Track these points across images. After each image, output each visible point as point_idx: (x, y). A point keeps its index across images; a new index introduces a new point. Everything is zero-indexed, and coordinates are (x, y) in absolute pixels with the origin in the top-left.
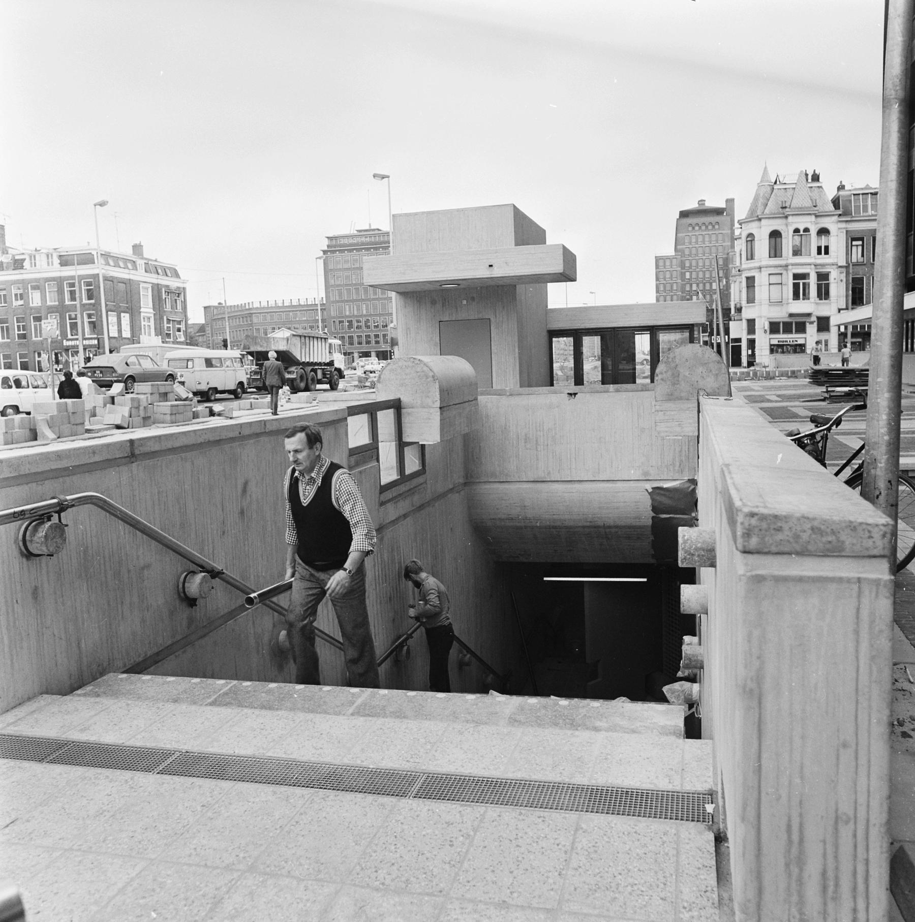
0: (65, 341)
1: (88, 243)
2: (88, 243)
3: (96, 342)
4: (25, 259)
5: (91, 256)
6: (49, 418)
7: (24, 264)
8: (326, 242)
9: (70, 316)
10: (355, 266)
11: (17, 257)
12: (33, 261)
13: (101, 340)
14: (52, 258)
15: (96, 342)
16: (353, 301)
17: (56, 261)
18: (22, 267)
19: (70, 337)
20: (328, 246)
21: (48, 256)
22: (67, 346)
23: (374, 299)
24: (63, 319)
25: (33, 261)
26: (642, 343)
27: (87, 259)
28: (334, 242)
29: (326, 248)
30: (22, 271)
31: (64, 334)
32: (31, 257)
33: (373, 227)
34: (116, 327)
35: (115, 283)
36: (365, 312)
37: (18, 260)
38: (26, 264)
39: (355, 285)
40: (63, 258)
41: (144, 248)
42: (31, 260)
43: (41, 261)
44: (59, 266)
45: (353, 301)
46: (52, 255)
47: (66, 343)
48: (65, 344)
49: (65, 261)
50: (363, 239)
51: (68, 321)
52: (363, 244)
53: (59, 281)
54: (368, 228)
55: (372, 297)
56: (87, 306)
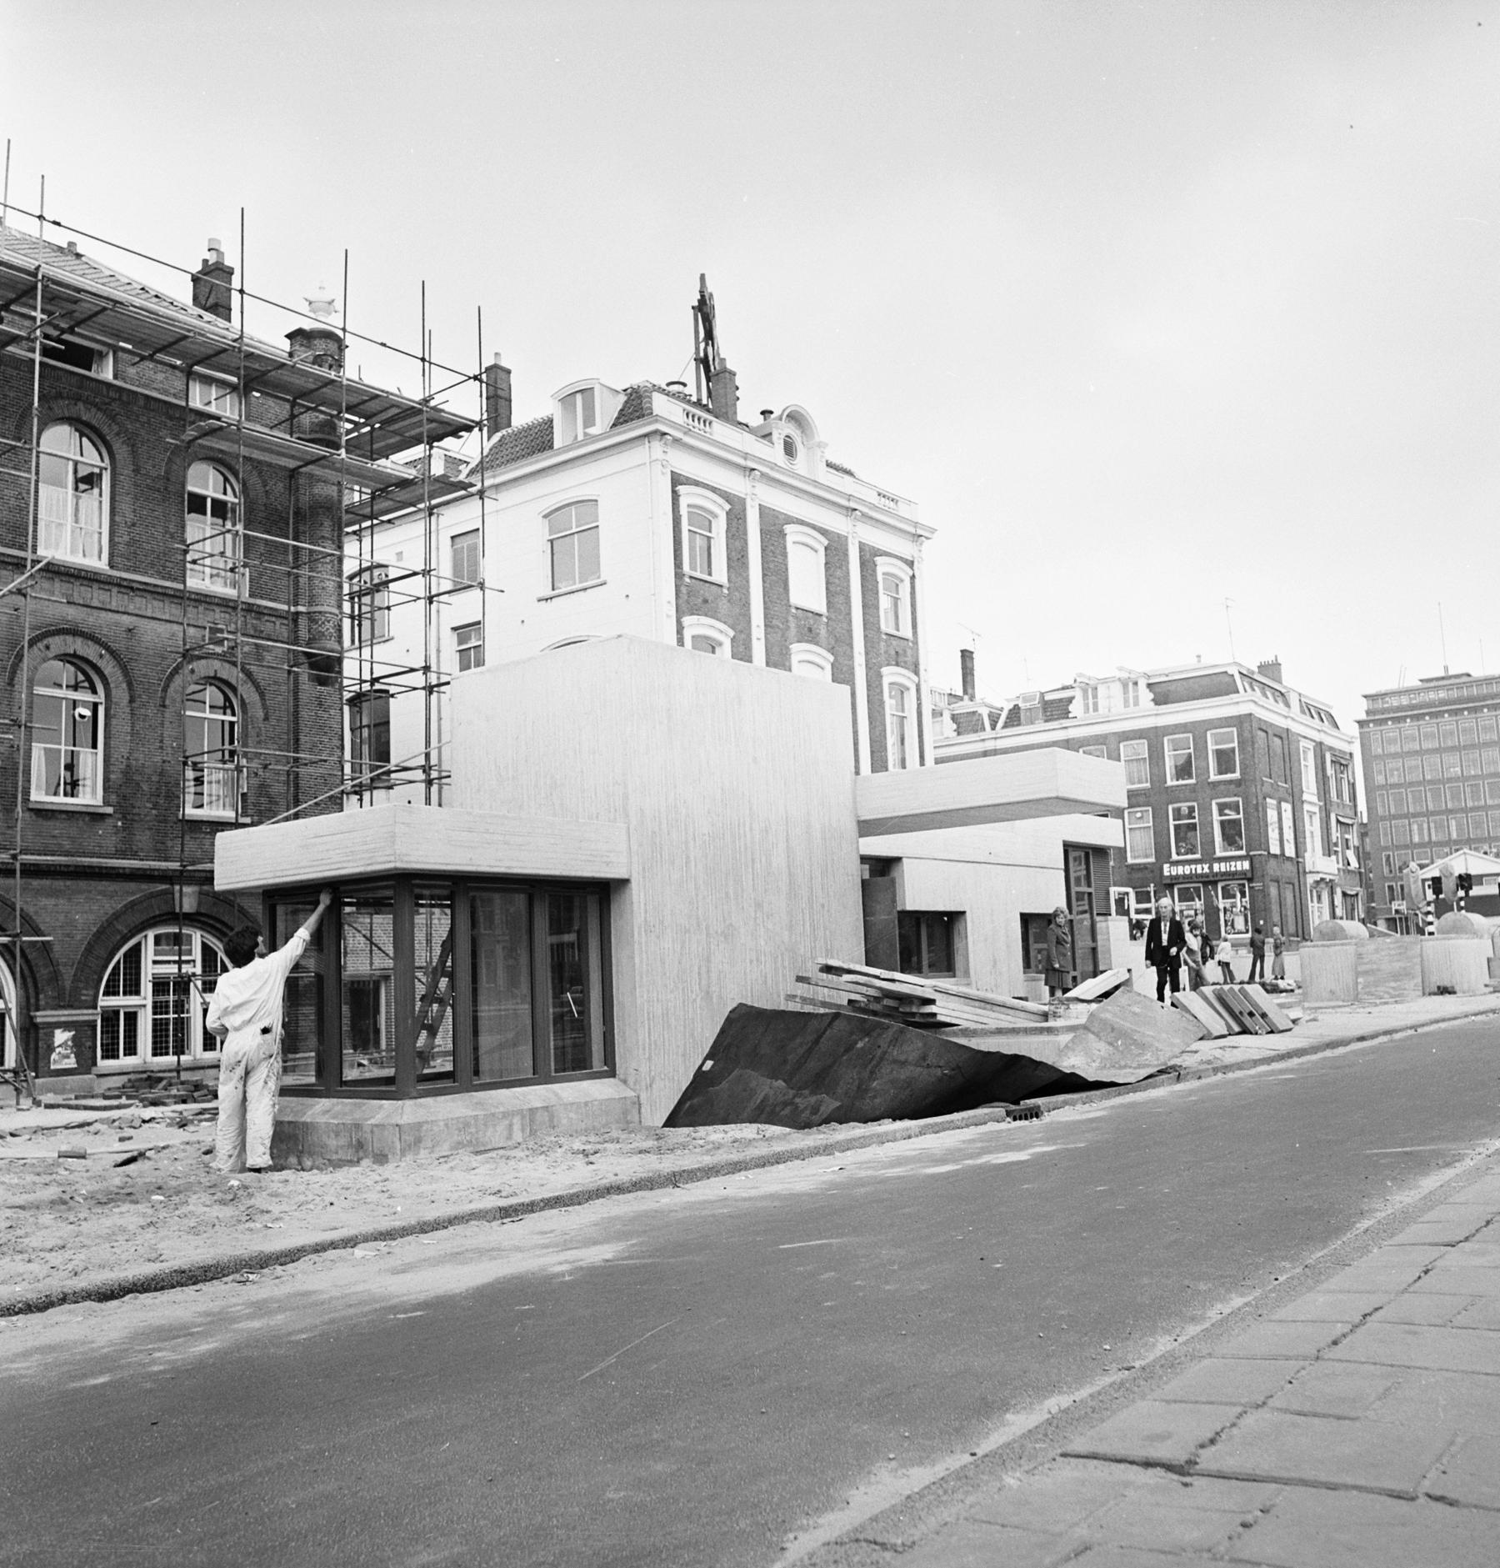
0: (1166, 867)
1: (1199, 656)
2: (1199, 656)
3: (1246, 865)
4: (1073, 698)
5: (1227, 679)
6: (372, 1050)
7: (1071, 708)
8: (1364, 705)
9: (1177, 812)
10: (1450, 744)
11: (1048, 697)
12: (1091, 701)
13: (1256, 861)
14: (1135, 691)
15: (1246, 865)
16: (1428, 814)
17: (1146, 696)
18: (1065, 714)
19: (1175, 857)
20: (1368, 713)
21: (1125, 686)
22: (1171, 877)
23: (1473, 809)
24: (1160, 818)
25: (1091, 701)
26: (580, 987)
27: (1218, 685)
28: (1379, 705)
29: (1363, 717)
30: (1065, 723)
31: (1162, 853)
32: (1085, 692)
33: (1452, 672)
34: (1277, 831)
35: (1270, 736)
36: (1454, 836)
37: (1052, 702)
38: (1076, 708)
39: (1431, 782)
40: (1158, 690)
41: (1283, 667)
42: (1085, 697)
43: (1111, 700)
44: (1152, 704)
45: (1428, 814)
46: (1136, 684)
47: (1167, 870)
48: (1166, 873)
49: (1163, 694)
50: (1432, 696)
51: (1172, 823)
52: (1443, 703)
53: (1154, 737)
54: (1442, 674)
55: (1470, 804)
56: (1222, 787)
